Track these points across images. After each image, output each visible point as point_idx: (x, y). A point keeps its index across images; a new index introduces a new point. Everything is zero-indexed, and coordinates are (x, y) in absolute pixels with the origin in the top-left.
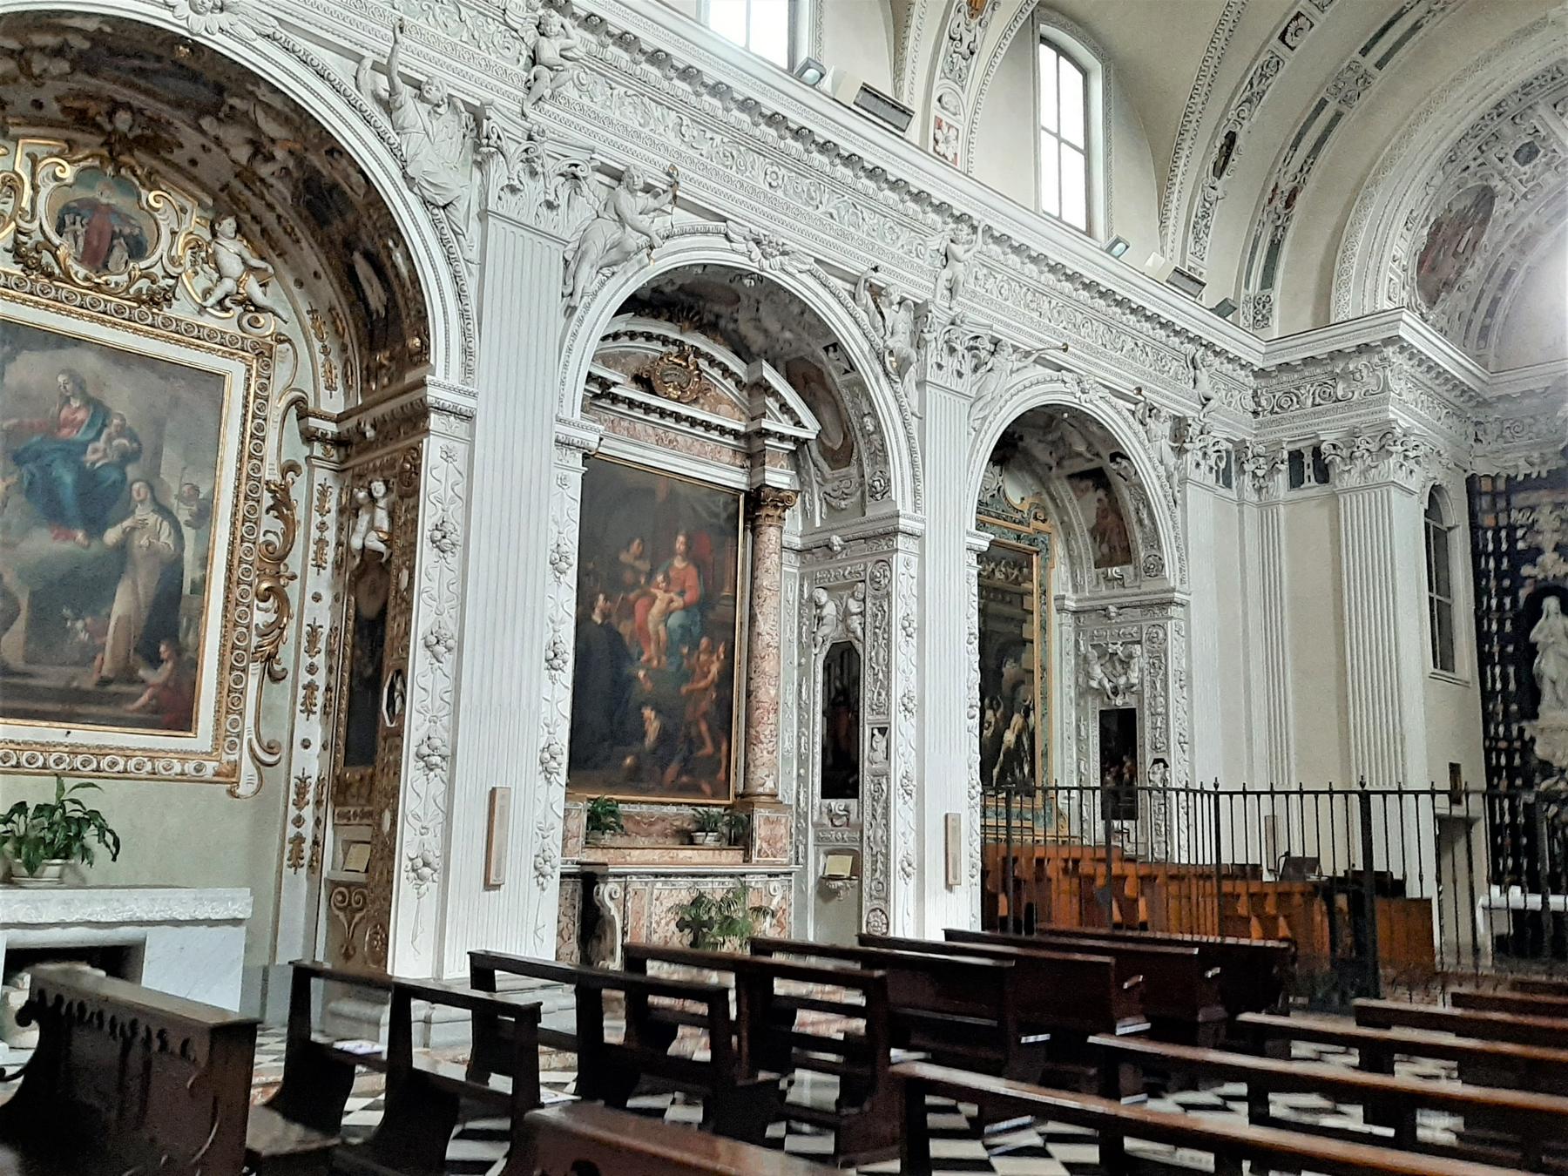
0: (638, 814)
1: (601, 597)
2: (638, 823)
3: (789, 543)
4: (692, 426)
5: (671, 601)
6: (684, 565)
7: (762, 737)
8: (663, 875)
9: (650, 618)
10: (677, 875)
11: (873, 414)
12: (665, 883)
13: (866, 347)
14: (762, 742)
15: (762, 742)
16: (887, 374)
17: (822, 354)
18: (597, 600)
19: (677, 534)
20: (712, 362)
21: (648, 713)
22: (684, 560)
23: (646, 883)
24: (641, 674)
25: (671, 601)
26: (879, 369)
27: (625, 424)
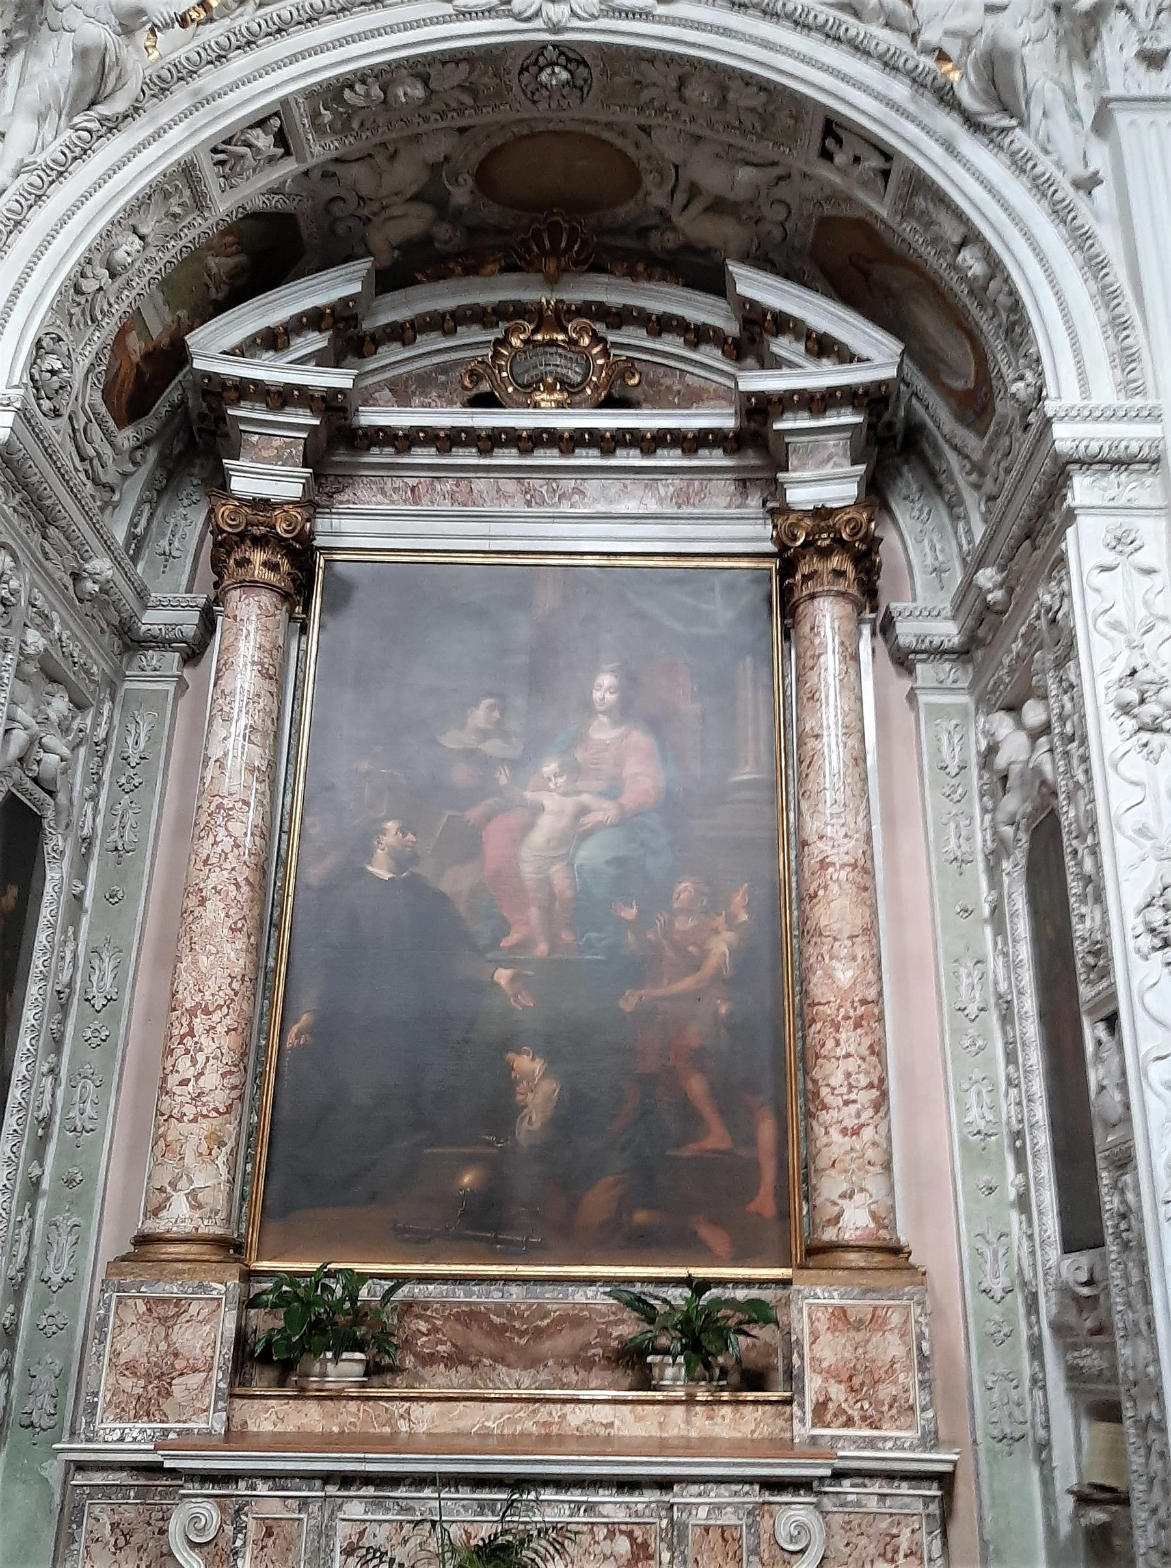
0: (500, 1309)
1: (391, 826)
2: (501, 1330)
3: (921, 638)
4: (608, 452)
5: (584, 810)
6: (615, 733)
7: (824, 1091)
8: (368, 1479)
9: (525, 853)
10: (420, 1481)
11: (971, 237)
12: (376, 1502)
13: (900, 90)
14: (825, 1107)
15: (825, 1107)
16: (972, 123)
17: (825, 172)
18: (383, 832)
19: (595, 670)
20: (661, 325)
21: (527, 1064)
22: (616, 724)
23: (304, 1502)
24: (503, 976)
25: (584, 810)
26: (949, 124)
27: (449, 486)
